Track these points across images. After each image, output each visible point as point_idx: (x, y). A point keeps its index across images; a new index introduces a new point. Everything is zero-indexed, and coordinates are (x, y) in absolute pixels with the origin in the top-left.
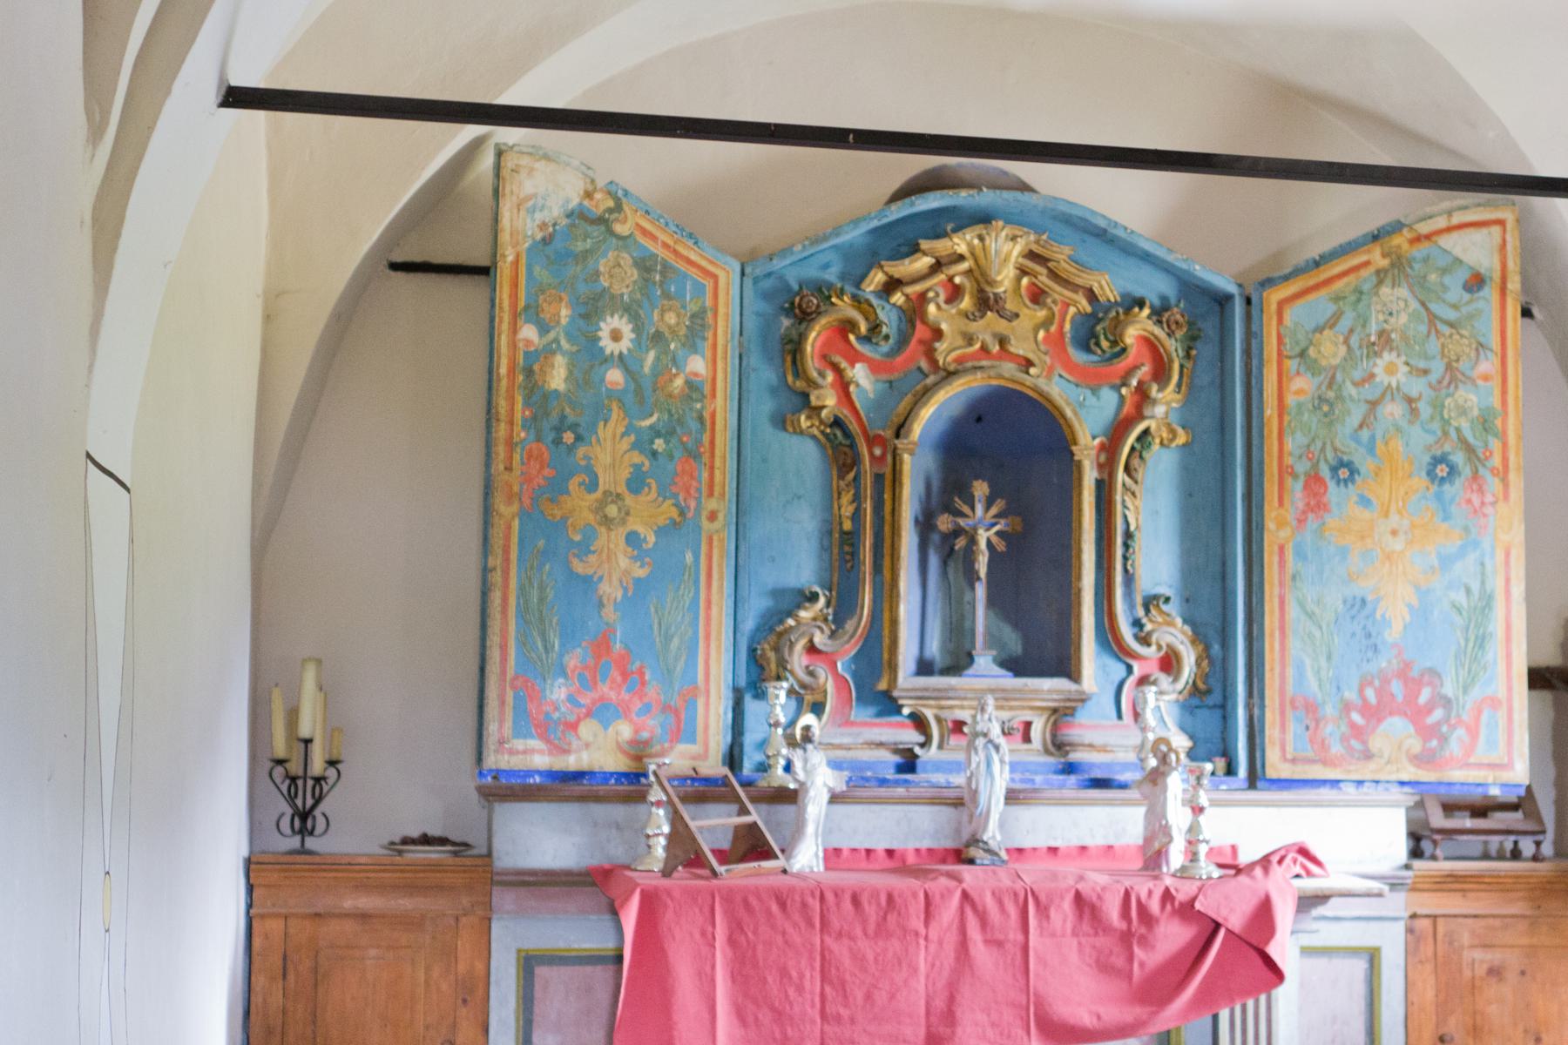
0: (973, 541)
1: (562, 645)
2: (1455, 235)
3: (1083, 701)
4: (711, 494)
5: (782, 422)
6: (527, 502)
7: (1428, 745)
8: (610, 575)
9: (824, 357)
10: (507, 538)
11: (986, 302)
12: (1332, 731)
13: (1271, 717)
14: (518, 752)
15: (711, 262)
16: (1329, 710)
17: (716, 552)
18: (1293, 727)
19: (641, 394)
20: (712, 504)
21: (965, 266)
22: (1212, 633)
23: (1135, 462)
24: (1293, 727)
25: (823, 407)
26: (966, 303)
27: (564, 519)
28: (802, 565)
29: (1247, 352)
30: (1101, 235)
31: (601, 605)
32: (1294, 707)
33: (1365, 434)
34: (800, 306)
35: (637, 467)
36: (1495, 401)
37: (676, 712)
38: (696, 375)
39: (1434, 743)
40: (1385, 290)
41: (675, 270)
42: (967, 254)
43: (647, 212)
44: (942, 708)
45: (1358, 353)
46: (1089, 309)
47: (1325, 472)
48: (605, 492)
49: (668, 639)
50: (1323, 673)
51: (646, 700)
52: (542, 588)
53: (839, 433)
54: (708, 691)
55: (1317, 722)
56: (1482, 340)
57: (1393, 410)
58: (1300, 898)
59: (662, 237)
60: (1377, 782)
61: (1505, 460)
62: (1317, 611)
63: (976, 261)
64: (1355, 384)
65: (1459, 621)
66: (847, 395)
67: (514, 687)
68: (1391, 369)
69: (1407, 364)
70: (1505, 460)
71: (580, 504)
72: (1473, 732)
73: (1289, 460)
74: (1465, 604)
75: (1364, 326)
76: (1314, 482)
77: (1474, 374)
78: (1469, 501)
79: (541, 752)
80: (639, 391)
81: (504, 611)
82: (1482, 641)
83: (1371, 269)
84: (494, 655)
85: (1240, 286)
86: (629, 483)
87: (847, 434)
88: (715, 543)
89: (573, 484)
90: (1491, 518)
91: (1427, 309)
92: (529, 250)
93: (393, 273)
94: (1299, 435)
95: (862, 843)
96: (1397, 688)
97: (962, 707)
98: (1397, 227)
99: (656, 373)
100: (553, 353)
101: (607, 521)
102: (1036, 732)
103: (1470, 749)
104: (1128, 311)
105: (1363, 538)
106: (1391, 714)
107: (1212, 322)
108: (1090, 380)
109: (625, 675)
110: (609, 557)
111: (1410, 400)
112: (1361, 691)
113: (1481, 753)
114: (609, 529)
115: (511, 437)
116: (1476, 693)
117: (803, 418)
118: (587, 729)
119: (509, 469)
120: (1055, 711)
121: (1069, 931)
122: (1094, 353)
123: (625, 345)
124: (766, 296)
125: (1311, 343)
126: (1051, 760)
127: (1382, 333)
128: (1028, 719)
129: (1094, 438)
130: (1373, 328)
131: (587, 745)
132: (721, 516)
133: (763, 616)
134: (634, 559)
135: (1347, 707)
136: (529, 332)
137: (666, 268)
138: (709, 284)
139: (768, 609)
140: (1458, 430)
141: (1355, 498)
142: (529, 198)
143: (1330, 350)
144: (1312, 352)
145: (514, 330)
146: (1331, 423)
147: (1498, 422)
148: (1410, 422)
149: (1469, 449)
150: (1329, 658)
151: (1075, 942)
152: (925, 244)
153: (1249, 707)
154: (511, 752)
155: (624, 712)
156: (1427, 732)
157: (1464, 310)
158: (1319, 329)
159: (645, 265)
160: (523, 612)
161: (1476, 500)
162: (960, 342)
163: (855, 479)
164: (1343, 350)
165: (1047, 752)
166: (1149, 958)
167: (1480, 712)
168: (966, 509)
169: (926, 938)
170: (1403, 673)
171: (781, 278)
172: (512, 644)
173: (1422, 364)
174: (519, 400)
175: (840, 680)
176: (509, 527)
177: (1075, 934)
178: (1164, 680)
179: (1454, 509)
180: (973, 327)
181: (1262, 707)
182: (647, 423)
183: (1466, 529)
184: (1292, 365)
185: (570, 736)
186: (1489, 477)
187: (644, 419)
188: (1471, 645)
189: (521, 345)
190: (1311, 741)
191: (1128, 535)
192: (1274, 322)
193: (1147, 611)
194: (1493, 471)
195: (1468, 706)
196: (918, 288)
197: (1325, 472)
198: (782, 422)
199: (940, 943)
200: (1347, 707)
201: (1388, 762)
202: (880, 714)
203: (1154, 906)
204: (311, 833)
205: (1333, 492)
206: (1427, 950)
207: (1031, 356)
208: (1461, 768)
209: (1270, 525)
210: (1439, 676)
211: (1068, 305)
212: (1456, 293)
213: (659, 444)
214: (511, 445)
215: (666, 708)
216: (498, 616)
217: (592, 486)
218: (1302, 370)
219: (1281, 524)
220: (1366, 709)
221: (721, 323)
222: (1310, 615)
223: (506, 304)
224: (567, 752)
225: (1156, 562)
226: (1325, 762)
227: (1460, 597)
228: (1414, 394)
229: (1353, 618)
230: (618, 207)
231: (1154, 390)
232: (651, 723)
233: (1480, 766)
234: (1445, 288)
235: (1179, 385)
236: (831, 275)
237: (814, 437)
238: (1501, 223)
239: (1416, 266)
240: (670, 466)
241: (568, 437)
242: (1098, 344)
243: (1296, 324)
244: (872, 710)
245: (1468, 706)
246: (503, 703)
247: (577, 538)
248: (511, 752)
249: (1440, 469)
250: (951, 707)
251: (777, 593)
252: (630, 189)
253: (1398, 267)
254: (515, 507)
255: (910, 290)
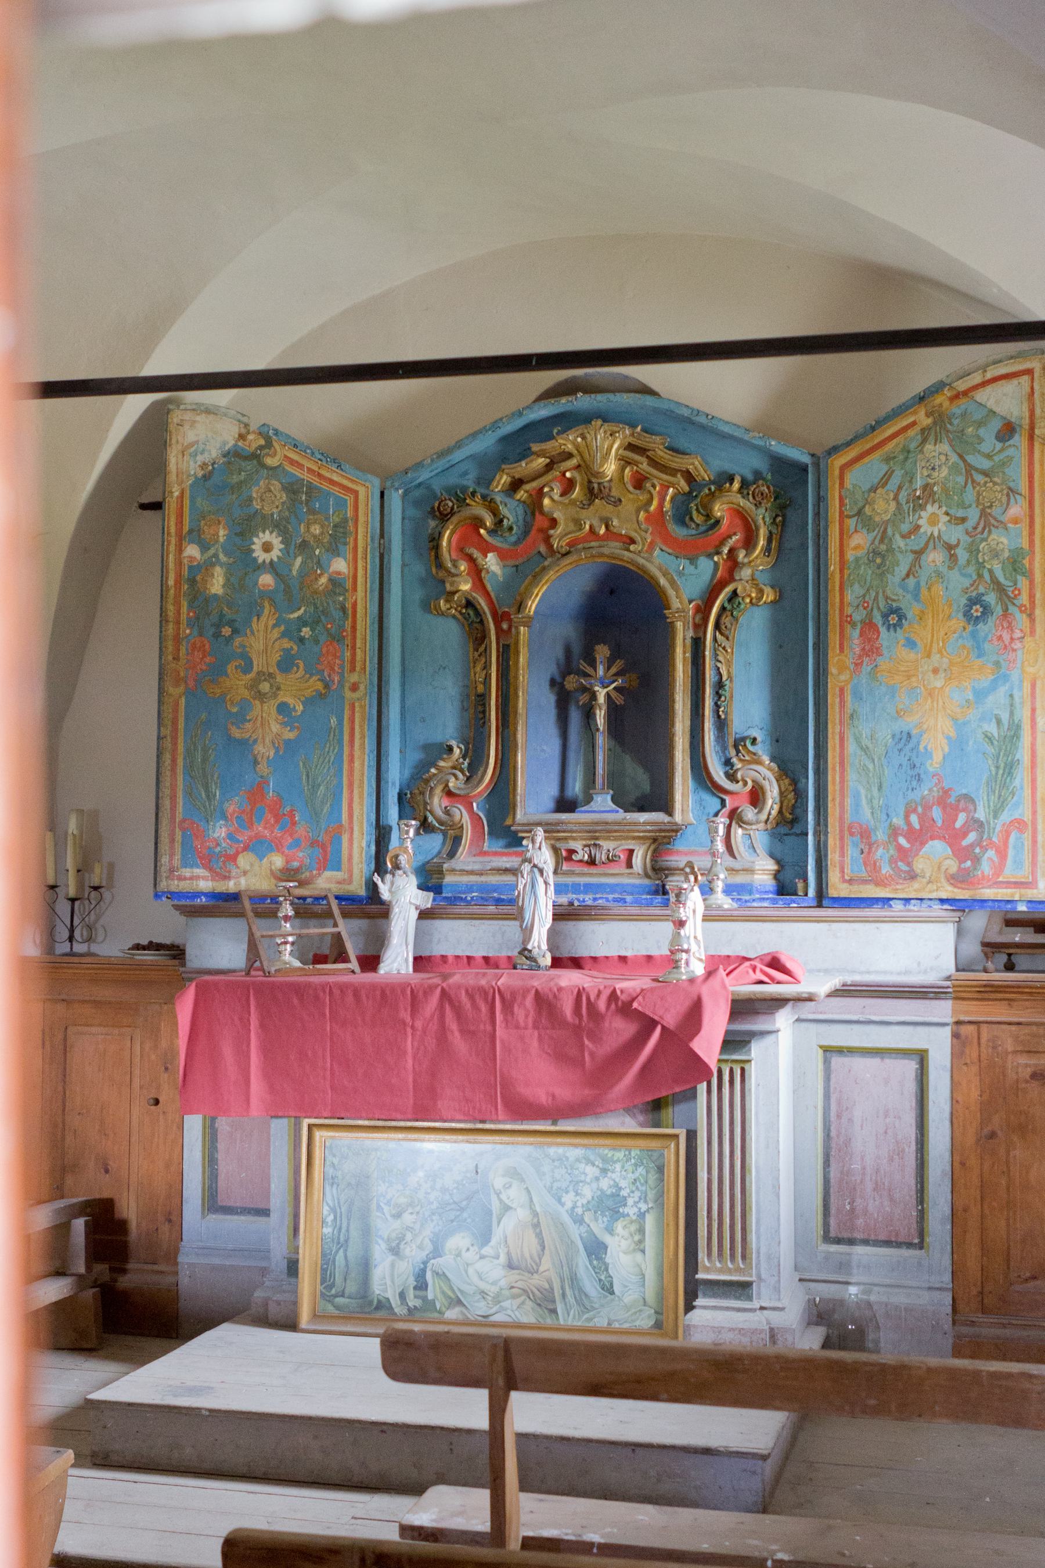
0: (594, 696)
1: (223, 794)
2: (989, 389)
3: (677, 831)
4: (353, 669)
5: (428, 606)
6: (191, 684)
7: (963, 866)
8: (263, 738)
9: (461, 550)
10: (176, 711)
11: (593, 493)
12: (882, 855)
13: (832, 841)
14: (185, 879)
15: (352, 481)
16: (880, 835)
17: (357, 715)
18: (852, 852)
19: (289, 592)
20: (354, 678)
21: (574, 462)
22: (790, 771)
23: (726, 620)
24: (852, 852)
25: (457, 591)
26: (577, 492)
27: (223, 695)
28: (446, 725)
29: (817, 514)
30: (694, 425)
31: (256, 762)
32: (852, 834)
33: (911, 581)
34: (438, 509)
35: (287, 651)
36: (1025, 545)
37: (323, 847)
38: (339, 573)
39: (969, 863)
40: (929, 447)
41: (319, 490)
42: (575, 452)
43: (295, 446)
44: (559, 839)
45: (905, 507)
46: (687, 489)
47: (878, 619)
48: (258, 673)
49: (315, 787)
50: (875, 802)
51: (296, 836)
52: (205, 750)
53: (471, 613)
54: (352, 829)
55: (870, 845)
56: (1012, 484)
57: (935, 558)
58: (734, 1001)
59: (307, 464)
60: (921, 899)
61: (1032, 597)
62: (870, 746)
63: (582, 457)
64: (903, 537)
65: (991, 750)
66: (481, 580)
67: (183, 830)
68: (933, 521)
69: (947, 514)
70: (1032, 597)
71: (237, 683)
72: (1002, 855)
73: (849, 611)
74: (996, 735)
75: (910, 482)
76: (869, 625)
77: (1004, 518)
78: (1000, 638)
79: (204, 878)
80: (288, 591)
81: (173, 770)
82: (1010, 768)
83: (917, 429)
84: (166, 803)
85: (813, 455)
86: (279, 664)
87: (478, 613)
88: (357, 709)
89: (230, 668)
90: (1019, 653)
91: (964, 461)
92: (191, 486)
93: (140, 511)
94: (856, 586)
95: (463, 951)
96: (937, 813)
97: (574, 839)
98: (938, 387)
99: (303, 574)
100: (213, 565)
101: (261, 696)
102: (637, 860)
103: (999, 869)
104: (720, 488)
105: (909, 677)
106: (932, 838)
107: (790, 489)
108: (689, 551)
109: (278, 818)
110: (262, 724)
111: (949, 547)
112: (907, 817)
113: (1009, 872)
114: (262, 703)
115: (178, 634)
116: (1005, 817)
117: (442, 602)
118: (244, 861)
119: (176, 658)
120: (655, 840)
121: (530, 1025)
122: (688, 527)
123: (275, 554)
124: (417, 503)
125: (867, 502)
126: (647, 882)
127: (926, 487)
128: (631, 847)
129: (690, 602)
130: (919, 483)
131: (245, 873)
132: (362, 687)
133: (416, 767)
134: (284, 724)
135: (894, 832)
136: (192, 551)
137: (311, 487)
138: (350, 499)
139: (421, 761)
140: (991, 571)
141: (902, 642)
142: (192, 445)
143: (883, 508)
144: (867, 510)
145: (180, 550)
146: (883, 574)
147: (1026, 562)
148: (950, 568)
149: (1000, 589)
150: (880, 788)
151: (536, 1033)
152: (535, 447)
153: (817, 833)
154: (181, 878)
155: (277, 846)
156: (963, 854)
157: (996, 458)
158: (874, 489)
159: (293, 489)
160: (189, 768)
161: (1006, 637)
162: (572, 527)
163: (486, 649)
164: (893, 504)
165: (647, 876)
166: (597, 1050)
167: (1008, 834)
168: (589, 670)
169: (413, 1027)
170: (942, 800)
171: (429, 488)
172: (180, 795)
173: (960, 513)
174: (185, 604)
175: (475, 818)
176: (177, 704)
177: (536, 1027)
178: (749, 813)
179: (987, 646)
180: (584, 514)
181: (826, 833)
182: (296, 615)
183: (997, 664)
184: (851, 523)
185: (230, 866)
186: (1018, 615)
187: (292, 613)
188: (1001, 772)
189: (185, 561)
190: (865, 864)
191: (720, 685)
192: (837, 486)
193: (738, 751)
194: (1022, 608)
195: (998, 828)
196: (535, 484)
197: (878, 619)
198: (428, 606)
199: (424, 1032)
200: (894, 832)
201: (929, 882)
202: (509, 845)
203: (602, 1005)
204: (94, 941)
205: (885, 636)
206: (972, 1053)
207: (633, 534)
208: (990, 887)
209: (833, 670)
210: (973, 801)
211: (668, 487)
212: (990, 443)
213: (306, 631)
214: (177, 640)
215: (314, 843)
216: (168, 773)
217: (248, 667)
218: (859, 526)
219: (842, 669)
220: (911, 834)
221: (361, 530)
222: (865, 750)
223: (173, 530)
224: (229, 878)
225: (750, 709)
226: (879, 883)
227: (992, 729)
228: (953, 542)
229: (900, 750)
230: (269, 444)
231: (741, 555)
232: (301, 854)
233: (1008, 884)
234: (981, 440)
235: (767, 550)
236: (469, 482)
237: (454, 616)
238: (1029, 372)
239: (956, 422)
240: (316, 649)
241: (226, 631)
242: (691, 519)
243: (855, 486)
244: (502, 842)
245: (998, 828)
246: (172, 841)
247: (235, 710)
248: (181, 878)
249: (975, 610)
250: (566, 839)
251: (427, 747)
252: (281, 429)
253: (940, 424)
254: (181, 689)
255: (527, 487)
